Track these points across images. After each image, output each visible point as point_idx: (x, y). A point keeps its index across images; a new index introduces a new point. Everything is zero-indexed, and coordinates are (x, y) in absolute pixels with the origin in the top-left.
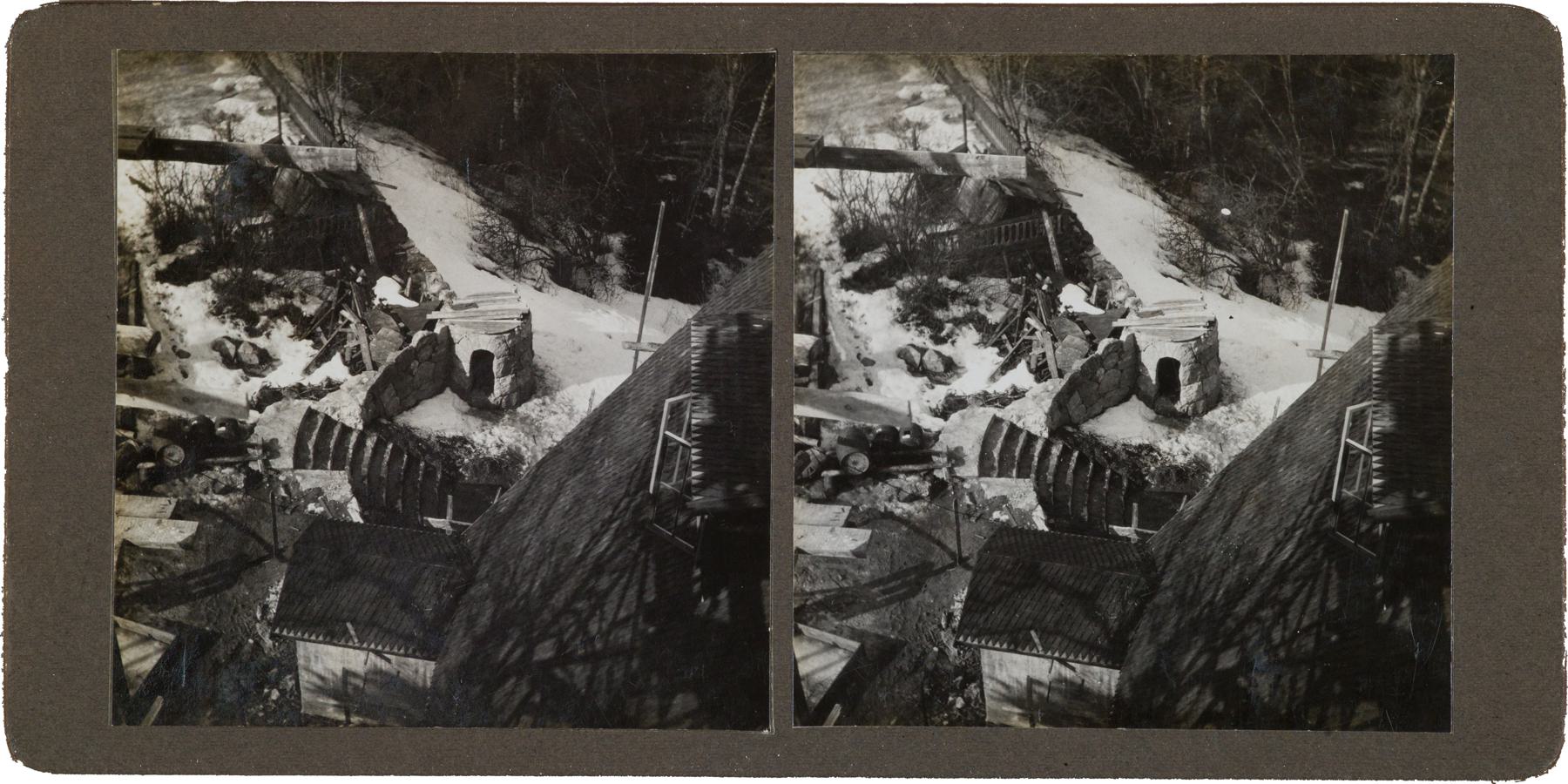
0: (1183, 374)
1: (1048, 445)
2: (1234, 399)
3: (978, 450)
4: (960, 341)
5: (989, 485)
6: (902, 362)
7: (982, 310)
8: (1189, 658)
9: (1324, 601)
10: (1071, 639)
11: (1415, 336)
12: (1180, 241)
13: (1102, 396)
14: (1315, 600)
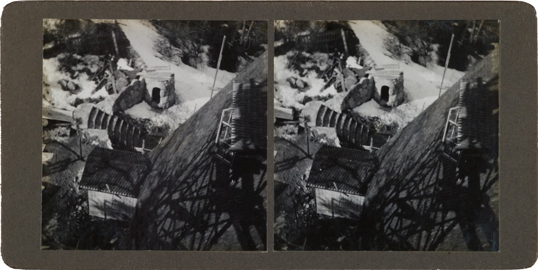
0: (162, 93)
1: (113, 118)
3: (87, 119)
4: (310, 76)
5: (319, 130)
7: (318, 65)
8: (162, 195)
10: (120, 187)
11: (249, 85)
13: (361, 98)
14: (435, 176)
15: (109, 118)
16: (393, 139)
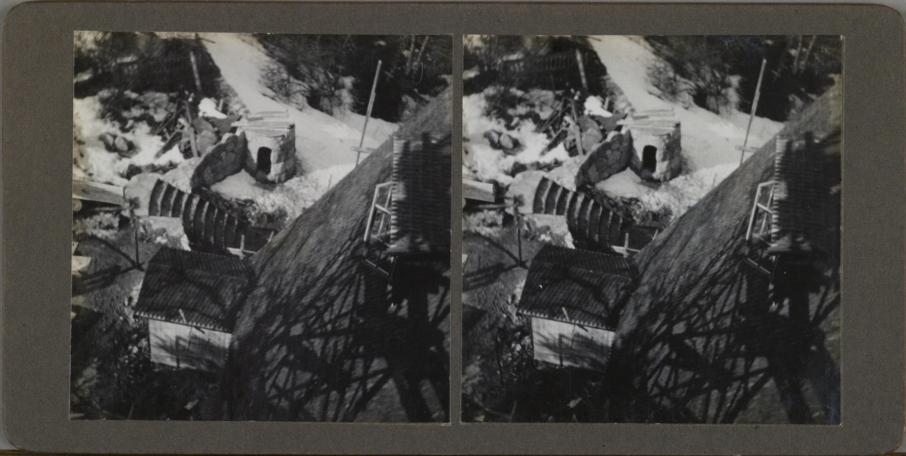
0: (659, 156)
1: (575, 195)
2: (688, 172)
3: (148, 200)
4: (523, 129)
5: (539, 219)
6: (101, 143)
7: (537, 110)
9: (738, 297)
11: (420, 143)
12: (660, 73)
14: (350, 298)
15: (570, 196)
16: (663, 235)
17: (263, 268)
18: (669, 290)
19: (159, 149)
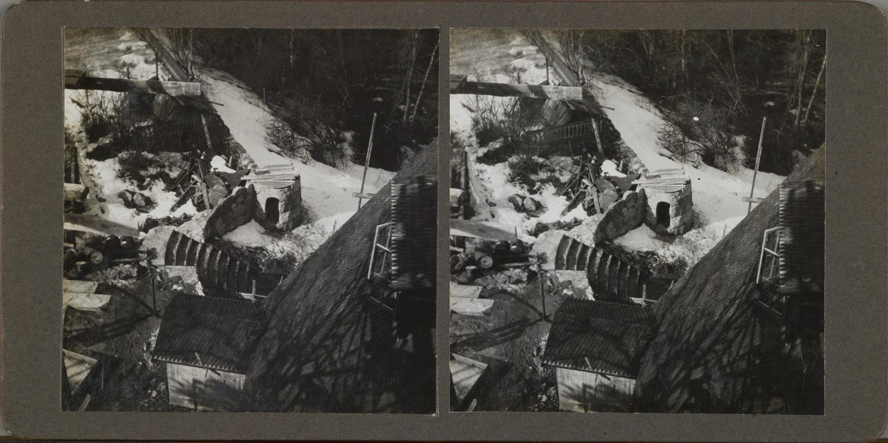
2: (700, 225)
4: (545, 192)
6: (511, 204)
7: (557, 175)
12: (670, 136)
13: (626, 224)
14: (747, 340)
15: (589, 252)
16: (679, 284)
17: (663, 315)
18: (686, 337)
19: (565, 208)
